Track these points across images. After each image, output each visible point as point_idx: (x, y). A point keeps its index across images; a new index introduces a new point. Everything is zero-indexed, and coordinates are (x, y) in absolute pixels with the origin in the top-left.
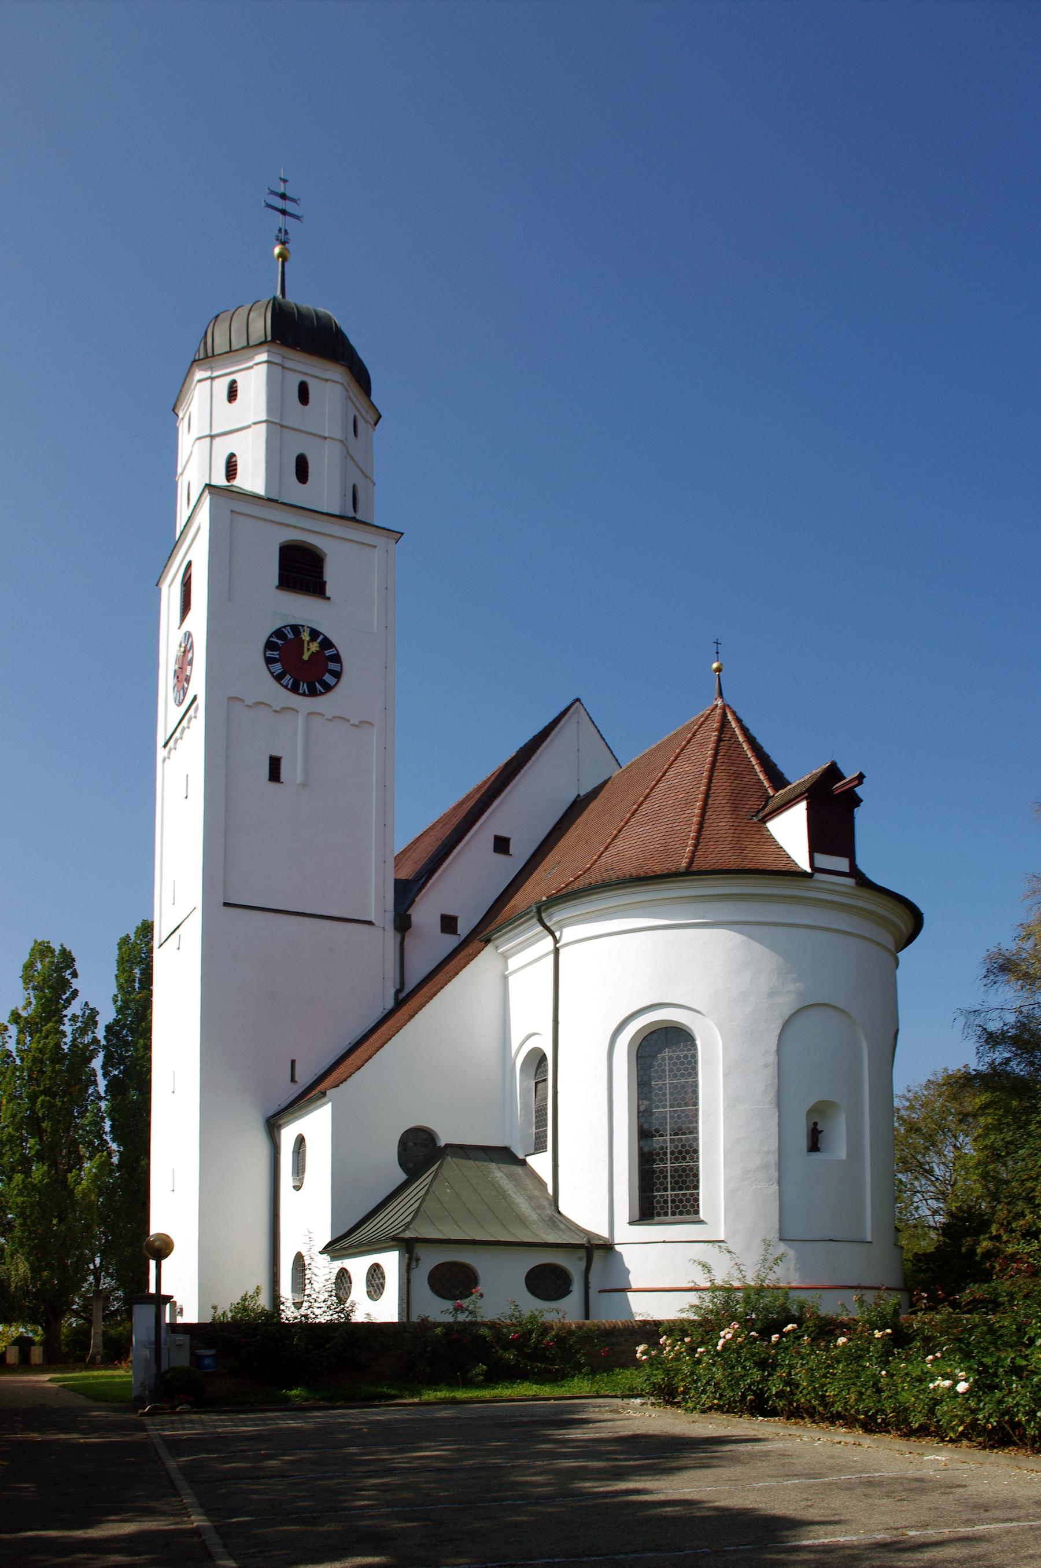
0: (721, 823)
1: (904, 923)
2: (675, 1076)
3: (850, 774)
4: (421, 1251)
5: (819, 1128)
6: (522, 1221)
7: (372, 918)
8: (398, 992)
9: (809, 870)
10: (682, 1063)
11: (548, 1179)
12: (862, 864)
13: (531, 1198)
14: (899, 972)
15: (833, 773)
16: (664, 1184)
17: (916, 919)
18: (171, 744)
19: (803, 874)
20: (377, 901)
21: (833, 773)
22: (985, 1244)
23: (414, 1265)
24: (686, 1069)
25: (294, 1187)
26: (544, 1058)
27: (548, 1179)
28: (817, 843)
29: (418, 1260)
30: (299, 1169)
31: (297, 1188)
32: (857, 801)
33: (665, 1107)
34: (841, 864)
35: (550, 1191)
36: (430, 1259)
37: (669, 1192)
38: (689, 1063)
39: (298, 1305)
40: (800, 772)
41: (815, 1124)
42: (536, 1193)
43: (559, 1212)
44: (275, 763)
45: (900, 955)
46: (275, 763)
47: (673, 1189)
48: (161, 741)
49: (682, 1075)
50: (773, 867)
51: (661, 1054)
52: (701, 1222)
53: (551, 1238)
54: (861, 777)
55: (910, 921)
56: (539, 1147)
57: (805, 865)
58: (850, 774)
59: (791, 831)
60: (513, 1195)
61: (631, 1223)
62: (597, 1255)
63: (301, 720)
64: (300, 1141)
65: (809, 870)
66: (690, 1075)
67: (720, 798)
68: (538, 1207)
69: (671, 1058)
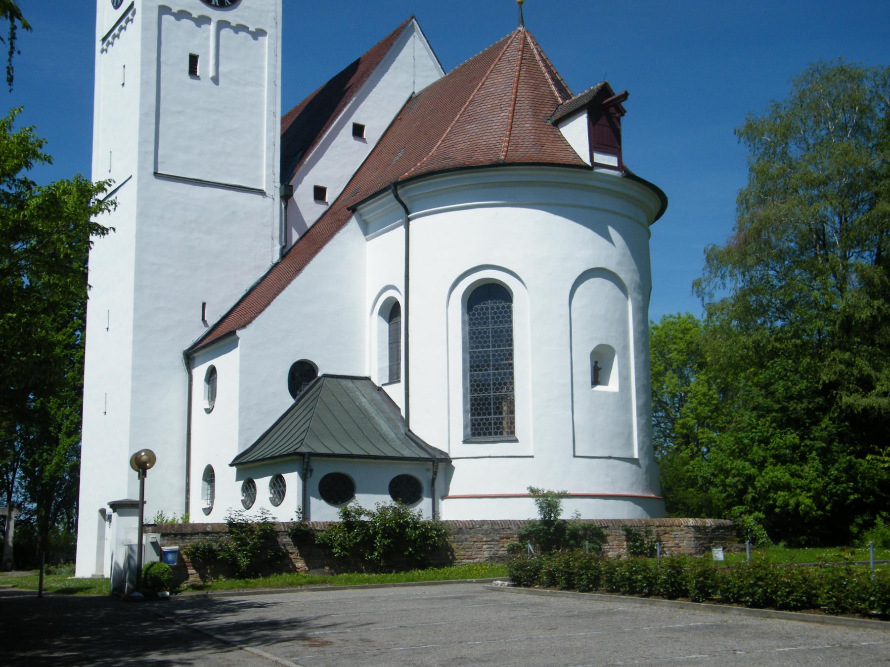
0: (526, 125)
1: (655, 206)
2: (496, 322)
3: (618, 91)
4: (315, 464)
5: (599, 366)
6: (384, 438)
7: (263, 187)
8: (283, 248)
9: (589, 164)
10: (501, 313)
11: (401, 404)
12: (625, 162)
13: (389, 420)
14: (651, 241)
15: (605, 90)
16: (490, 410)
17: (663, 201)
18: (110, 39)
19: (586, 167)
20: (266, 169)
21: (605, 90)
22: (876, 303)
23: (309, 475)
24: (503, 317)
25: (206, 410)
26: (397, 305)
27: (401, 404)
28: (596, 145)
29: (311, 471)
30: (212, 395)
31: (208, 411)
32: (622, 112)
33: (488, 347)
34: (613, 161)
35: (403, 414)
36: (321, 471)
37: (492, 416)
38: (506, 312)
39: (208, 511)
40: (581, 91)
41: (596, 362)
42: (392, 415)
43: (410, 431)
44: (193, 60)
45: (653, 228)
46: (193, 60)
47: (495, 414)
48: (100, 33)
49: (501, 322)
50: (564, 161)
51: (487, 303)
52: (516, 441)
53: (407, 453)
54: (625, 96)
55: (657, 202)
56: (394, 378)
57: (587, 160)
58: (618, 91)
59: (577, 134)
60: (376, 418)
61: (465, 442)
62: (441, 466)
63: (212, 27)
64: (212, 373)
65: (589, 164)
66: (506, 322)
67: (525, 107)
68: (394, 428)
69: (492, 308)
